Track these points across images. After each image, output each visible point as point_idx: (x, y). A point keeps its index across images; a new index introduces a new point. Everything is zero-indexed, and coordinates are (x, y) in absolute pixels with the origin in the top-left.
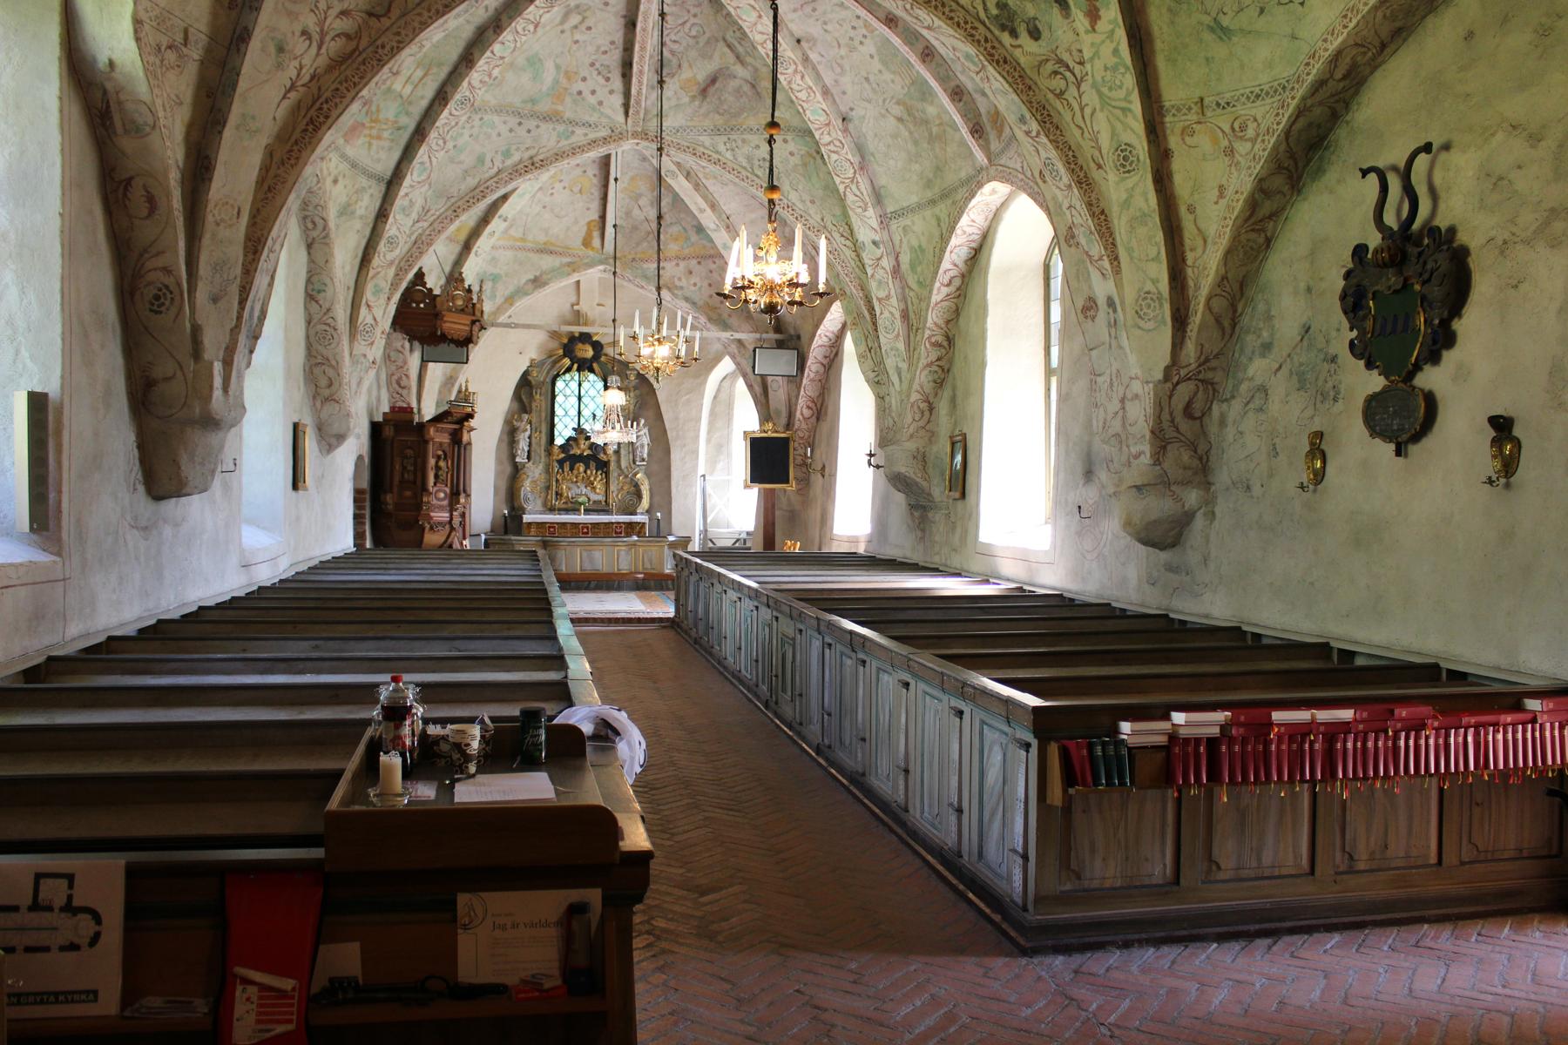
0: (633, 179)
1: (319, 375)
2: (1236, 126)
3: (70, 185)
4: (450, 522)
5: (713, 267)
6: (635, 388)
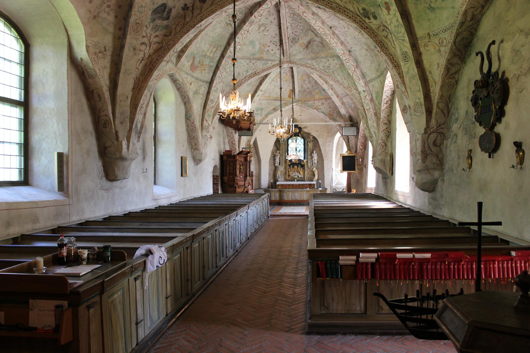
0: (302, 75)
2: (440, 42)
3: (71, 94)
5: (330, 101)
6: (312, 141)
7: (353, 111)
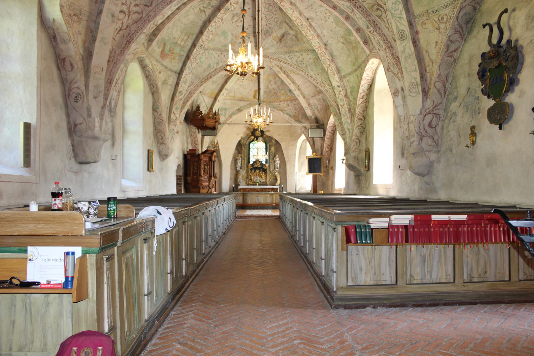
0: (268, 75)
1: (158, 135)
3: (41, 58)
4: (209, 186)
5: (295, 103)
6: (275, 145)
7: (319, 113)
